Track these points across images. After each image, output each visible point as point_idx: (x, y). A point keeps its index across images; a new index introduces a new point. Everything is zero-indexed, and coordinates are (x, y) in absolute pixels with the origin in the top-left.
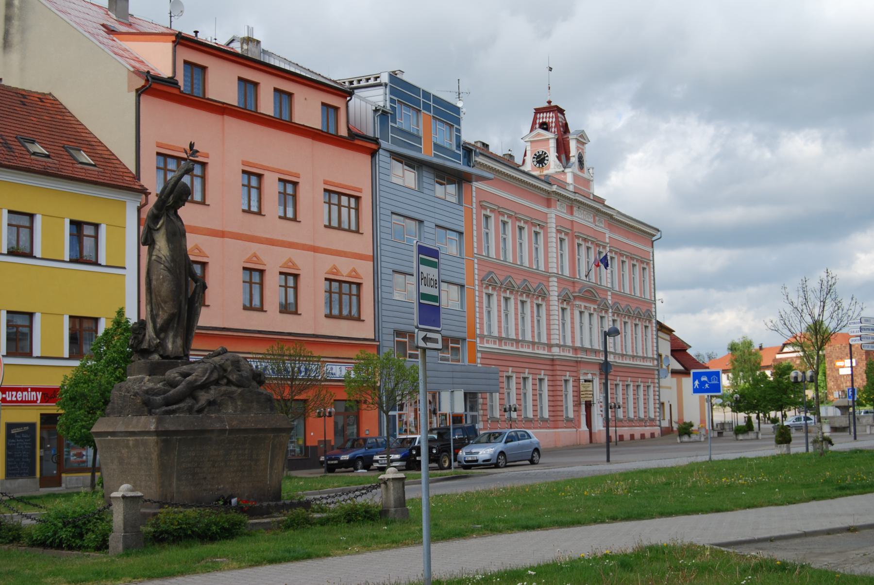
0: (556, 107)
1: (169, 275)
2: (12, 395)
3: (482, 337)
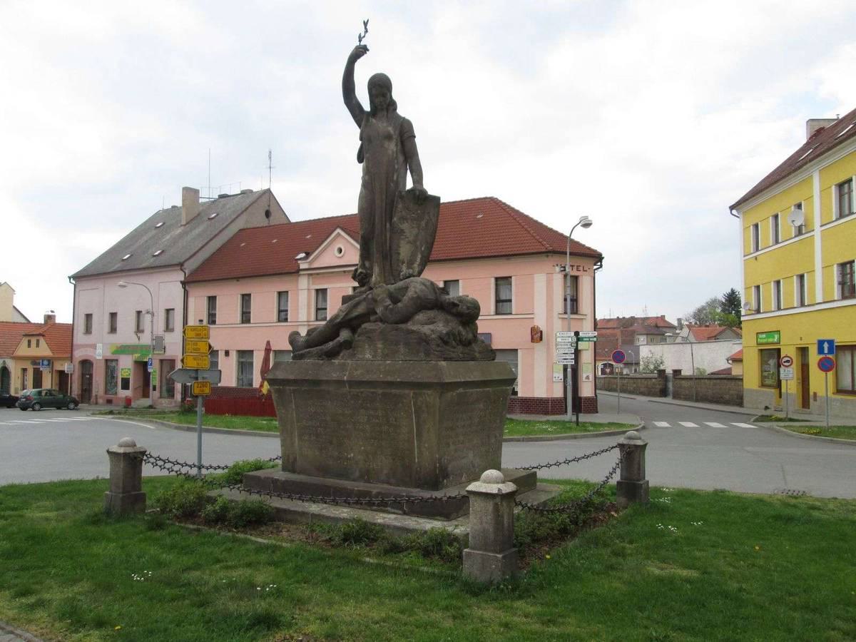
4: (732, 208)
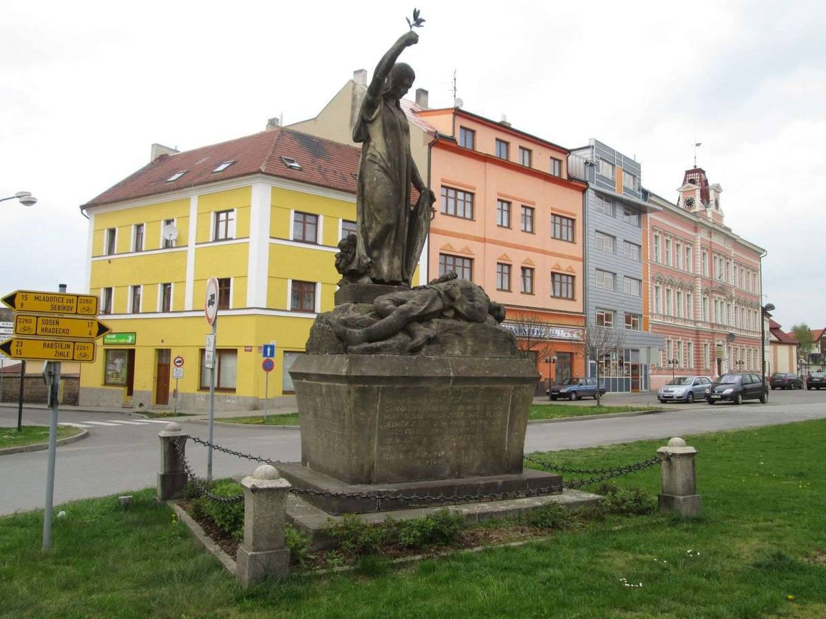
0: (700, 169)
3: (652, 315)
4: (83, 207)
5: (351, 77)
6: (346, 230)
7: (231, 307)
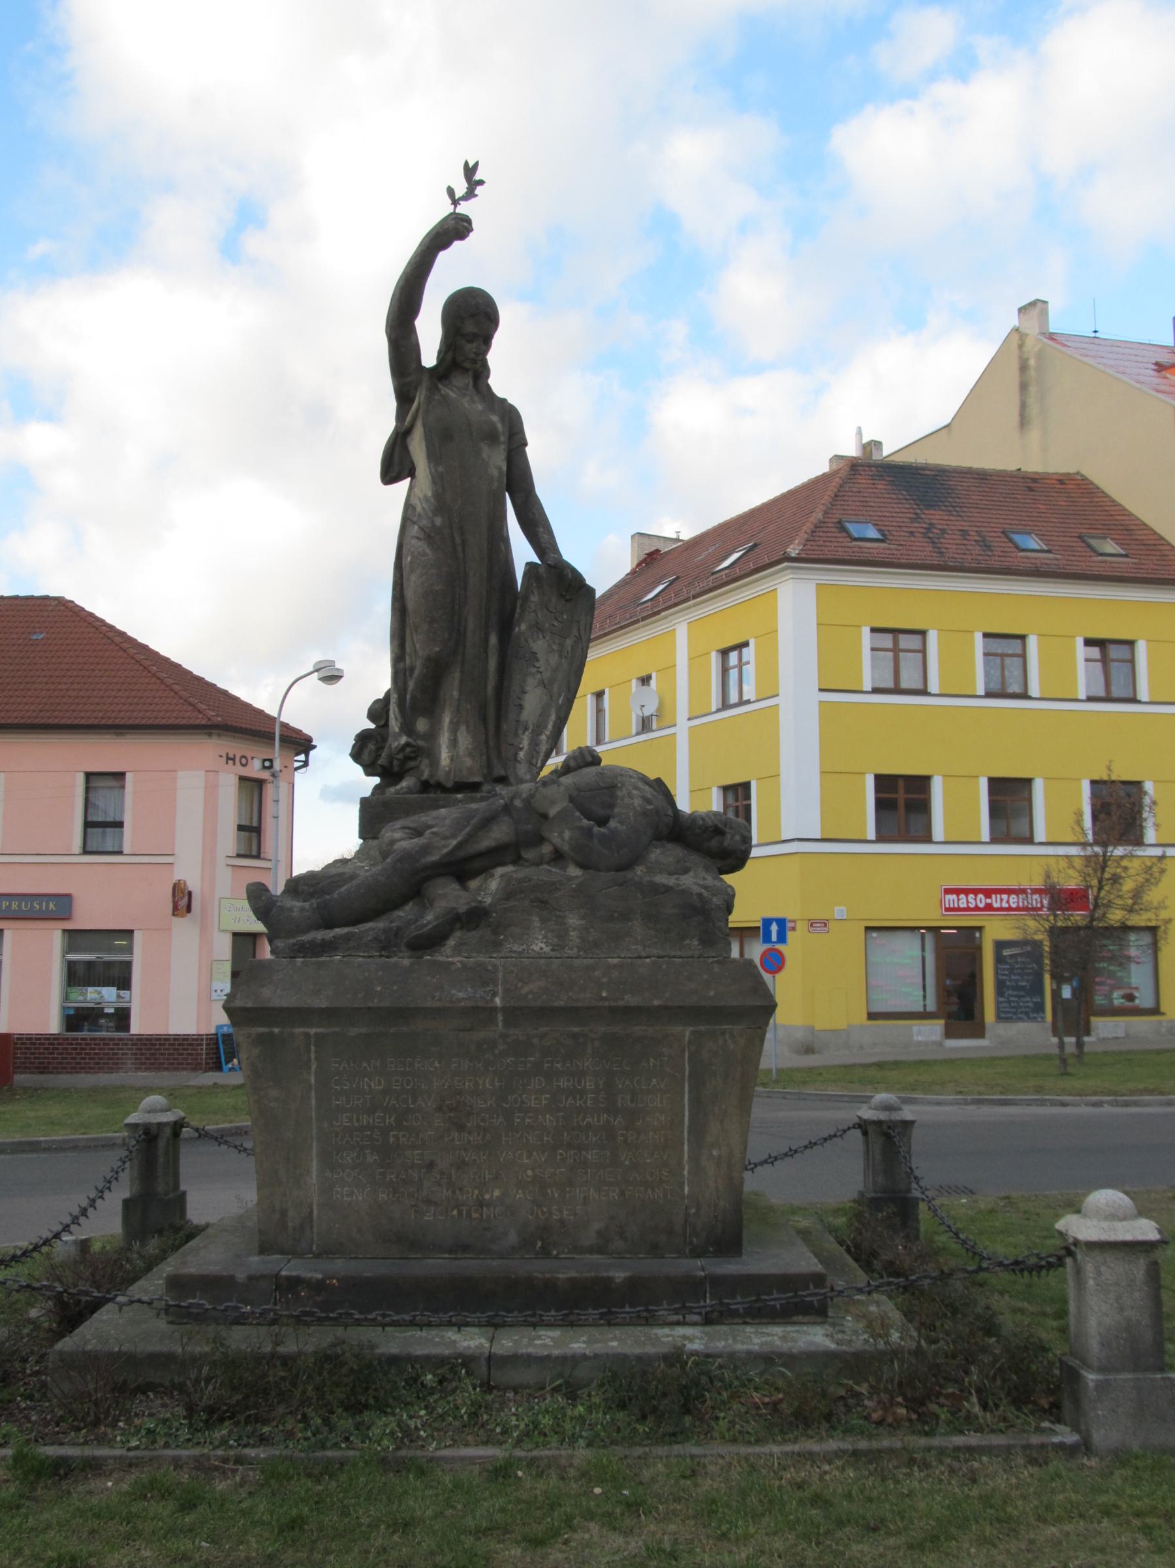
1: (427, 551)
2: (1002, 900)
5: (1014, 321)
6: (996, 655)
7: (938, 832)
